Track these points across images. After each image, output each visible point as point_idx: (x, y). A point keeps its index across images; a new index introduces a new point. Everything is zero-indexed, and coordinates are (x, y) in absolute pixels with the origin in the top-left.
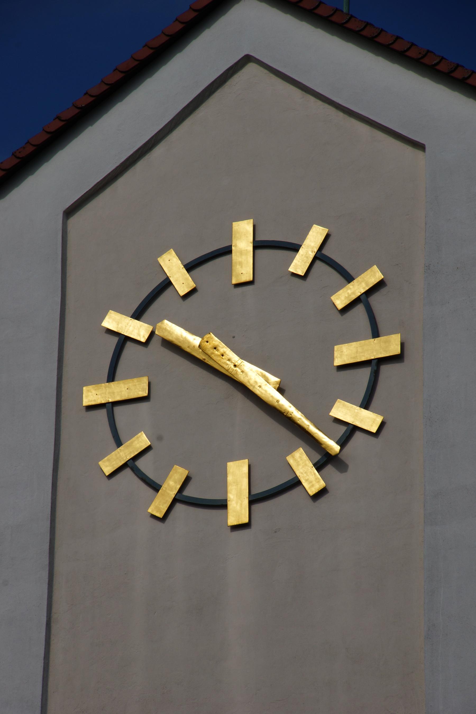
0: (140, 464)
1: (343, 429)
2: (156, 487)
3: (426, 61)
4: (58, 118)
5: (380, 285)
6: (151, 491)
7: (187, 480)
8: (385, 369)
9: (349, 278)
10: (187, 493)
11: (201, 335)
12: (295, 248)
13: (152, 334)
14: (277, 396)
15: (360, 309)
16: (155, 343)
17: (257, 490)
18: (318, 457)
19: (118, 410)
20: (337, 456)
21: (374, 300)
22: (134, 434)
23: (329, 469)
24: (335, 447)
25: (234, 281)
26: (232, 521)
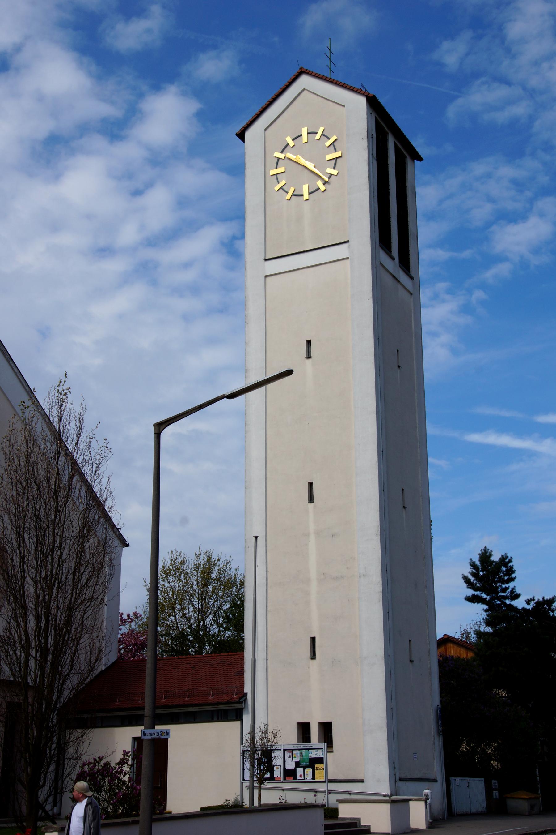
0: (284, 187)
1: (329, 175)
2: (287, 193)
3: (344, 86)
4: (262, 108)
5: (336, 140)
6: (286, 194)
7: (294, 190)
8: (338, 160)
9: (329, 139)
10: (294, 193)
11: (296, 155)
12: (316, 133)
13: (285, 157)
14: (389, 132)
15: (332, 146)
16: (286, 159)
17: (310, 191)
18: (324, 182)
19: (278, 175)
20: (328, 181)
21: (335, 144)
22: (282, 181)
23: (326, 184)
24: (327, 179)
25: (303, 142)
26: (305, 199)
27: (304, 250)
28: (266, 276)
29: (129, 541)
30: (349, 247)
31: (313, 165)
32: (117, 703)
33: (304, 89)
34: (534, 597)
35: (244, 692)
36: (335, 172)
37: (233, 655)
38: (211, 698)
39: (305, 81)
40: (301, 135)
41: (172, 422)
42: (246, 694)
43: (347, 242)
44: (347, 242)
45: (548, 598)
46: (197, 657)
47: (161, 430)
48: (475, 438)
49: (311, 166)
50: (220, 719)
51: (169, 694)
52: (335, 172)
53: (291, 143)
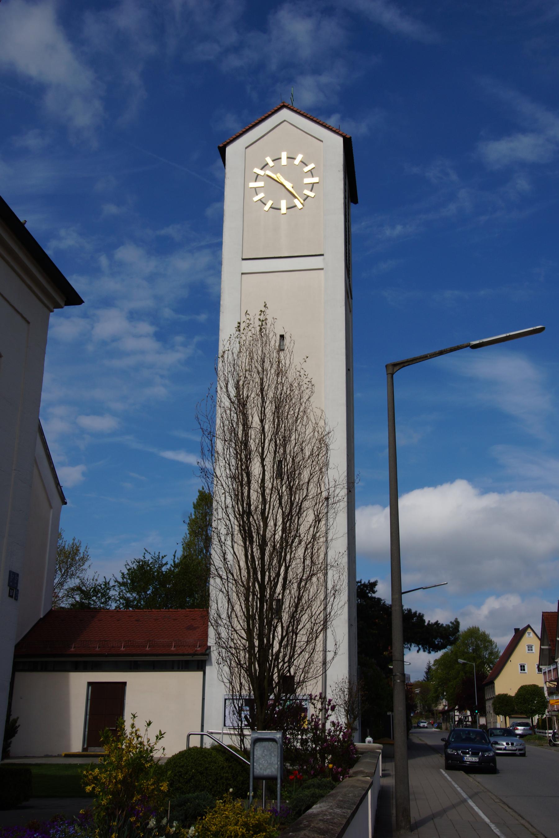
1: (306, 196)
13: (265, 174)
27: (280, 256)
28: (242, 274)
29: (67, 500)
30: (324, 259)
31: (292, 185)
32: (72, 649)
33: (285, 121)
34: (361, 580)
35: (207, 645)
36: (312, 194)
37: (174, 611)
38: (173, 649)
39: (285, 113)
40: (280, 158)
41: (416, 362)
42: (210, 647)
43: (322, 255)
44: (322, 255)
45: (372, 582)
46: (137, 612)
47: (395, 370)
48: (169, 455)
49: (289, 185)
50: (180, 669)
51: (131, 644)
52: (312, 194)
53: (271, 164)
